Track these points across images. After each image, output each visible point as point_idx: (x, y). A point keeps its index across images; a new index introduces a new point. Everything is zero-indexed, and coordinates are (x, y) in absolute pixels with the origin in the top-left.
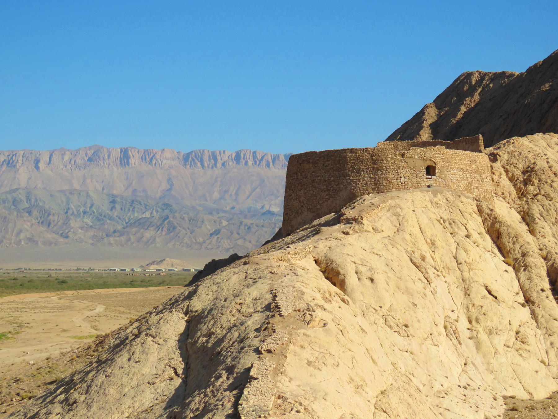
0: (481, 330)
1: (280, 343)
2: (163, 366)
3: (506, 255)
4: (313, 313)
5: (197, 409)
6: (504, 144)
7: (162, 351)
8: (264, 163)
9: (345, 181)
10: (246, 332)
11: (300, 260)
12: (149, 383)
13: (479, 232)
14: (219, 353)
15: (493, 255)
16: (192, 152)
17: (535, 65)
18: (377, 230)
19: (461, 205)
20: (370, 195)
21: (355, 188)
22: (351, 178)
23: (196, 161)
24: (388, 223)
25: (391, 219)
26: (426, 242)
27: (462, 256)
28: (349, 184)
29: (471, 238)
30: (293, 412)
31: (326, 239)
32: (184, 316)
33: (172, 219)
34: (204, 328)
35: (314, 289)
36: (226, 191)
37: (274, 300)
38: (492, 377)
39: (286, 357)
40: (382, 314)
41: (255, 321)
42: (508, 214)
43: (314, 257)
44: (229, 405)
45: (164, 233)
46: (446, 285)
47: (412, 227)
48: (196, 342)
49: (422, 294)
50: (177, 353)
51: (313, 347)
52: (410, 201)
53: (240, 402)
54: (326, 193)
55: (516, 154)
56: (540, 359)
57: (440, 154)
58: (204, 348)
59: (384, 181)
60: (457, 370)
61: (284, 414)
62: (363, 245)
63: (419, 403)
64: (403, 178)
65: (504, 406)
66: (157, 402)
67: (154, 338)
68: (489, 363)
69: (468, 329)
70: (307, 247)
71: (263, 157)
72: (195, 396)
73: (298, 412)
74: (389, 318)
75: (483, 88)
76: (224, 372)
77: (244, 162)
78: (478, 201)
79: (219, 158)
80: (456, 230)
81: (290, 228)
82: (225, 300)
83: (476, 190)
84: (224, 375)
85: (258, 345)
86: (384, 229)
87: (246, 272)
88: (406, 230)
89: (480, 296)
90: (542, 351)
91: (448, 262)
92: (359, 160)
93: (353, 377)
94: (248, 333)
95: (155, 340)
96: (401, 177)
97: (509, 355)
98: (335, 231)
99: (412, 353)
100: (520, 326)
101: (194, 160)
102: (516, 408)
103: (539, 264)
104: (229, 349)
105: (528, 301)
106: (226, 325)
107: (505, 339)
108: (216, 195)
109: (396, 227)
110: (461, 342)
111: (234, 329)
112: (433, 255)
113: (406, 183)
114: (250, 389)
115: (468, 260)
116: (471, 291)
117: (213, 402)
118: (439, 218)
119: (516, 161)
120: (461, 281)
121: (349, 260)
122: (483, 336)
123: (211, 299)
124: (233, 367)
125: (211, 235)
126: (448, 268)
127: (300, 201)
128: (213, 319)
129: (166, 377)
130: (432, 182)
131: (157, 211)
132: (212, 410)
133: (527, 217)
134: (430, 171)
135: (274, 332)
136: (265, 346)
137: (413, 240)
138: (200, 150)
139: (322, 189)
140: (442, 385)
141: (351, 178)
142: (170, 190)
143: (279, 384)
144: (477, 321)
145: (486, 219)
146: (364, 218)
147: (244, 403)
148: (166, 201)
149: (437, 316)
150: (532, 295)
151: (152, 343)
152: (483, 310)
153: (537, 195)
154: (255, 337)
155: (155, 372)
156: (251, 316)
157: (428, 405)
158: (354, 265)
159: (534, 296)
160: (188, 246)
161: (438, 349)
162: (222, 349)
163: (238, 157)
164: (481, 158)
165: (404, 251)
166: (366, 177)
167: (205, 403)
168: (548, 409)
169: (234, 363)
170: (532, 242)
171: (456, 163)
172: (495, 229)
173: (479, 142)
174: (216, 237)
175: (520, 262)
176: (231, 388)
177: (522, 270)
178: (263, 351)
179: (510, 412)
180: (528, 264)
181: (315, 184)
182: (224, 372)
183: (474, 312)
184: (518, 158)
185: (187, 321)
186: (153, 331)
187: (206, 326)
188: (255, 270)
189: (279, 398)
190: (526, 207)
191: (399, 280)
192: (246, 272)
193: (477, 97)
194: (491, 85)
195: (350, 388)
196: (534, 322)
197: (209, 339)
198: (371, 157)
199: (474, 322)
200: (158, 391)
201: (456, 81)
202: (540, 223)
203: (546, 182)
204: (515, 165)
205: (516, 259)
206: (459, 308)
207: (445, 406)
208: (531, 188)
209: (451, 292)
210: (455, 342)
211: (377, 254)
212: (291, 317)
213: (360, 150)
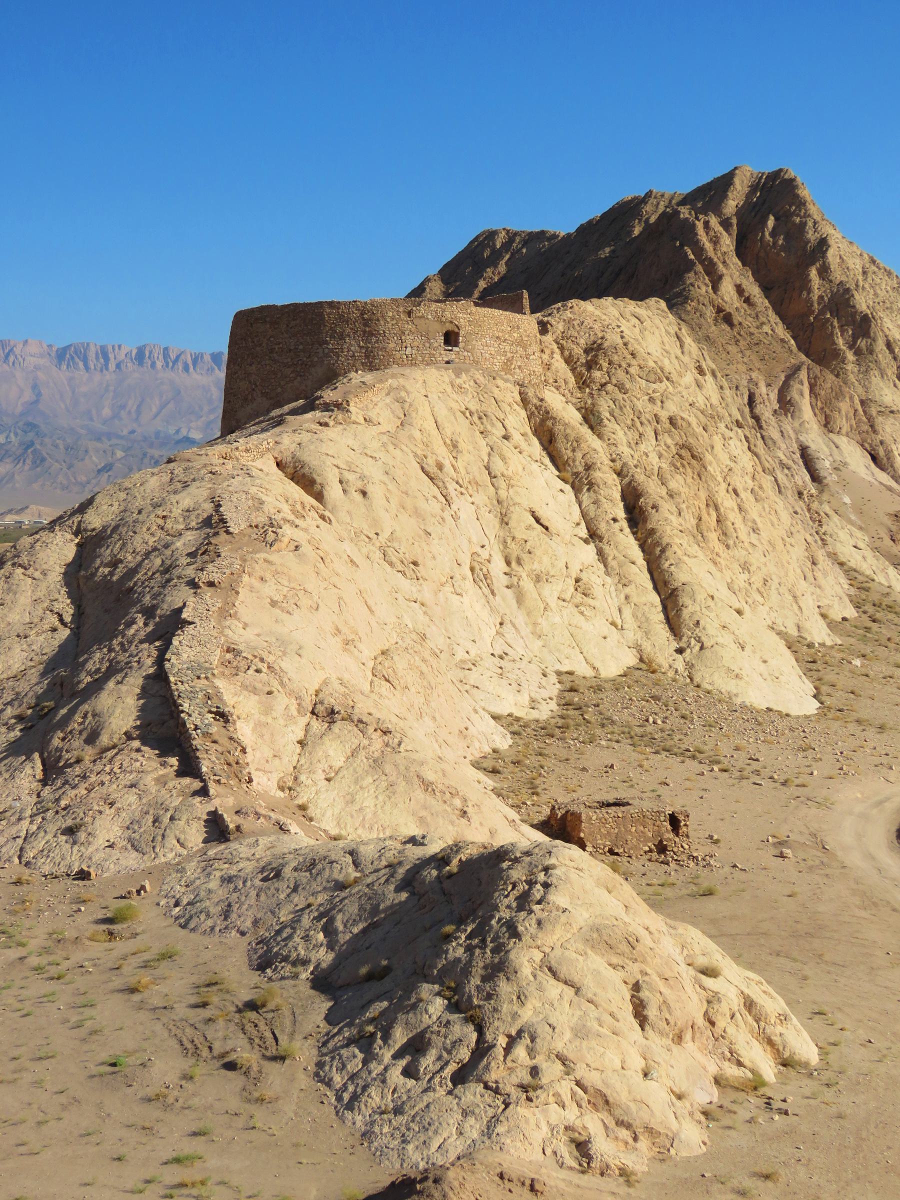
0: (524, 575)
1: (228, 572)
2: (41, 611)
3: (561, 467)
4: (279, 530)
5: (98, 670)
6: (558, 309)
8: (180, 365)
9: (320, 351)
10: (173, 558)
11: (253, 461)
12: (18, 636)
13: (522, 432)
14: (131, 590)
15: (543, 467)
16: (71, 345)
17: (590, 222)
18: (370, 421)
19: (496, 391)
20: (360, 372)
23: (77, 360)
24: (387, 413)
25: (392, 406)
27: (498, 466)
28: (327, 355)
29: (511, 440)
31: (294, 431)
32: (73, 536)
33: (38, 447)
34: (106, 554)
35: (279, 498)
36: (123, 407)
37: (217, 511)
38: (540, 643)
39: (237, 593)
40: (378, 545)
41: (187, 542)
42: (565, 410)
43: (276, 458)
44: (149, 662)
45: (27, 467)
46: (473, 507)
47: (423, 419)
48: (94, 575)
49: (438, 518)
50: (62, 592)
51: (279, 580)
52: (421, 382)
53: (167, 656)
54: (292, 369)
55: (576, 323)
56: (610, 620)
57: (464, 314)
58: (106, 583)
60: (489, 632)
61: (237, 675)
62: (351, 442)
63: (437, 673)
64: (409, 349)
65: (558, 686)
66: (32, 664)
67: (26, 569)
68: (535, 624)
69: (505, 574)
70: (265, 442)
71: (178, 357)
72: (94, 652)
73: (258, 671)
74: (390, 551)
75: (512, 254)
76: (140, 615)
77: (150, 363)
78: (522, 386)
79: (111, 356)
80: (489, 427)
81: (234, 423)
82: (140, 512)
83: (517, 370)
84: (140, 622)
85: (193, 576)
86: (381, 420)
87: (172, 473)
88: (414, 424)
89: (523, 525)
90: (612, 607)
92: (343, 319)
93: (340, 627)
94: (177, 560)
95: (27, 573)
97: (565, 612)
98: (307, 421)
99: (423, 605)
100: (581, 571)
101: (72, 358)
102: (576, 687)
103: (610, 482)
104: (147, 583)
105: (593, 536)
106: (141, 548)
107: (559, 589)
108: (107, 412)
109: (399, 418)
111: (154, 554)
112: (454, 462)
113: (414, 356)
114: (182, 637)
115: (505, 472)
116: (510, 518)
117: (123, 658)
118: (463, 409)
119: (576, 334)
120: (495, 502)
121: (328, 463)
122: (527, 584)
123: (117, 512)
124: (154, 607)
125: (99, 471)
126: (477, 483)
127: (250, 382)
128: (120, 539)
129: (47, 627)
130: (454, 356)
131: (16, 434)
132: (122, 670)
133: (591, 416)
134: (451, 338)
135: (219, 556)
136: (204, 577)
138: (83, 344)
139: (286, 362)
140: (467, 652)
142: (36, 402)
143: (227, 632)
144: (519, 562)
147: (173, 657)
148: (30, 419)
149: (460, 552)
150: (599, 526)
151: (22, 577)
152: (528, 546)
153: (605, 384)
154: (188, 564)
155: (28, 620)
156: (181, 535)
157: (449, 677)
158: (337, 470)
159: (602, 528)
160: (64, 488)
161: (462, 600)
162: (135, 584)
163: (140, 356)
164: (528, 322)
165: (411, 455)
166: (353, 345)
167: (110, 661)
168: (621, 691)
169: (155, 602)
170: (600, 450)
172: (546, 428)
173: (522, 302)
174: (106, 475)
175: (582, 478)
176: (150, 639)
177: (585, 490)
178: (201, 584)
179: (566, 694)
180: (593, 481)
182: (140, 615)
183: (514, 549)
185: (78, 545)
186: (24, 559)
187: (109, 551)
188: (185, 469)
189: (228, 651)
190: (589, 402)
191: (404, 495)
192: (172, 473)
193: (502, 268)
194: (524, 251)
195: (336, 643)
196: (602, 566)
197: (115, 569)
198: (362, 314)
199: (514, 564)
200: (34, 647)
201: (472, 242)
202: (610, 426)
203: (620, 366)
205: (577, 474)
206: (492, 541)
207: (472, 682)
208: (597, 374)
209: (480, 517)
210: (487, 591)
212: (245, 535)
213: (345, 304)
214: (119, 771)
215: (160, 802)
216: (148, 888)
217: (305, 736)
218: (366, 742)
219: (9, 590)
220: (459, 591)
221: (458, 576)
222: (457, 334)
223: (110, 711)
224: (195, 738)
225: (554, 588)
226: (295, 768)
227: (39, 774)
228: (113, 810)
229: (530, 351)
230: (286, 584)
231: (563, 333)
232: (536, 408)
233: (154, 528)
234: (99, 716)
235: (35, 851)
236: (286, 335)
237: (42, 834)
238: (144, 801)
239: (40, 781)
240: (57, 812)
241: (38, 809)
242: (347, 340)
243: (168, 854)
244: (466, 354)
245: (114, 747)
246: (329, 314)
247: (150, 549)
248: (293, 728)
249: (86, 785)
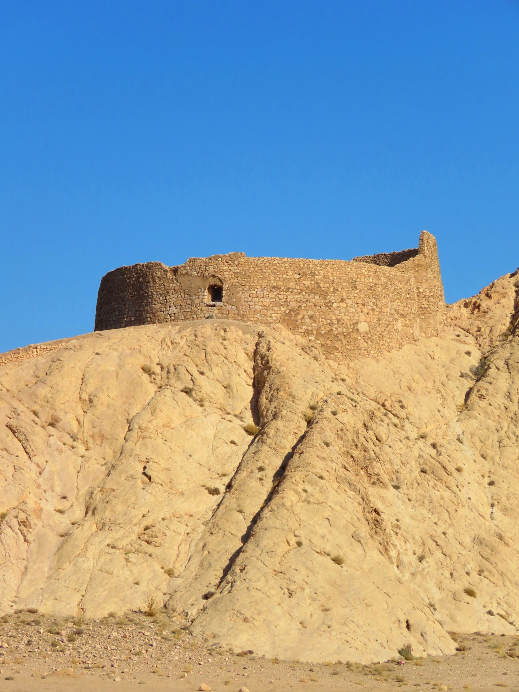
13: (225, 383)
83: (308, 321)
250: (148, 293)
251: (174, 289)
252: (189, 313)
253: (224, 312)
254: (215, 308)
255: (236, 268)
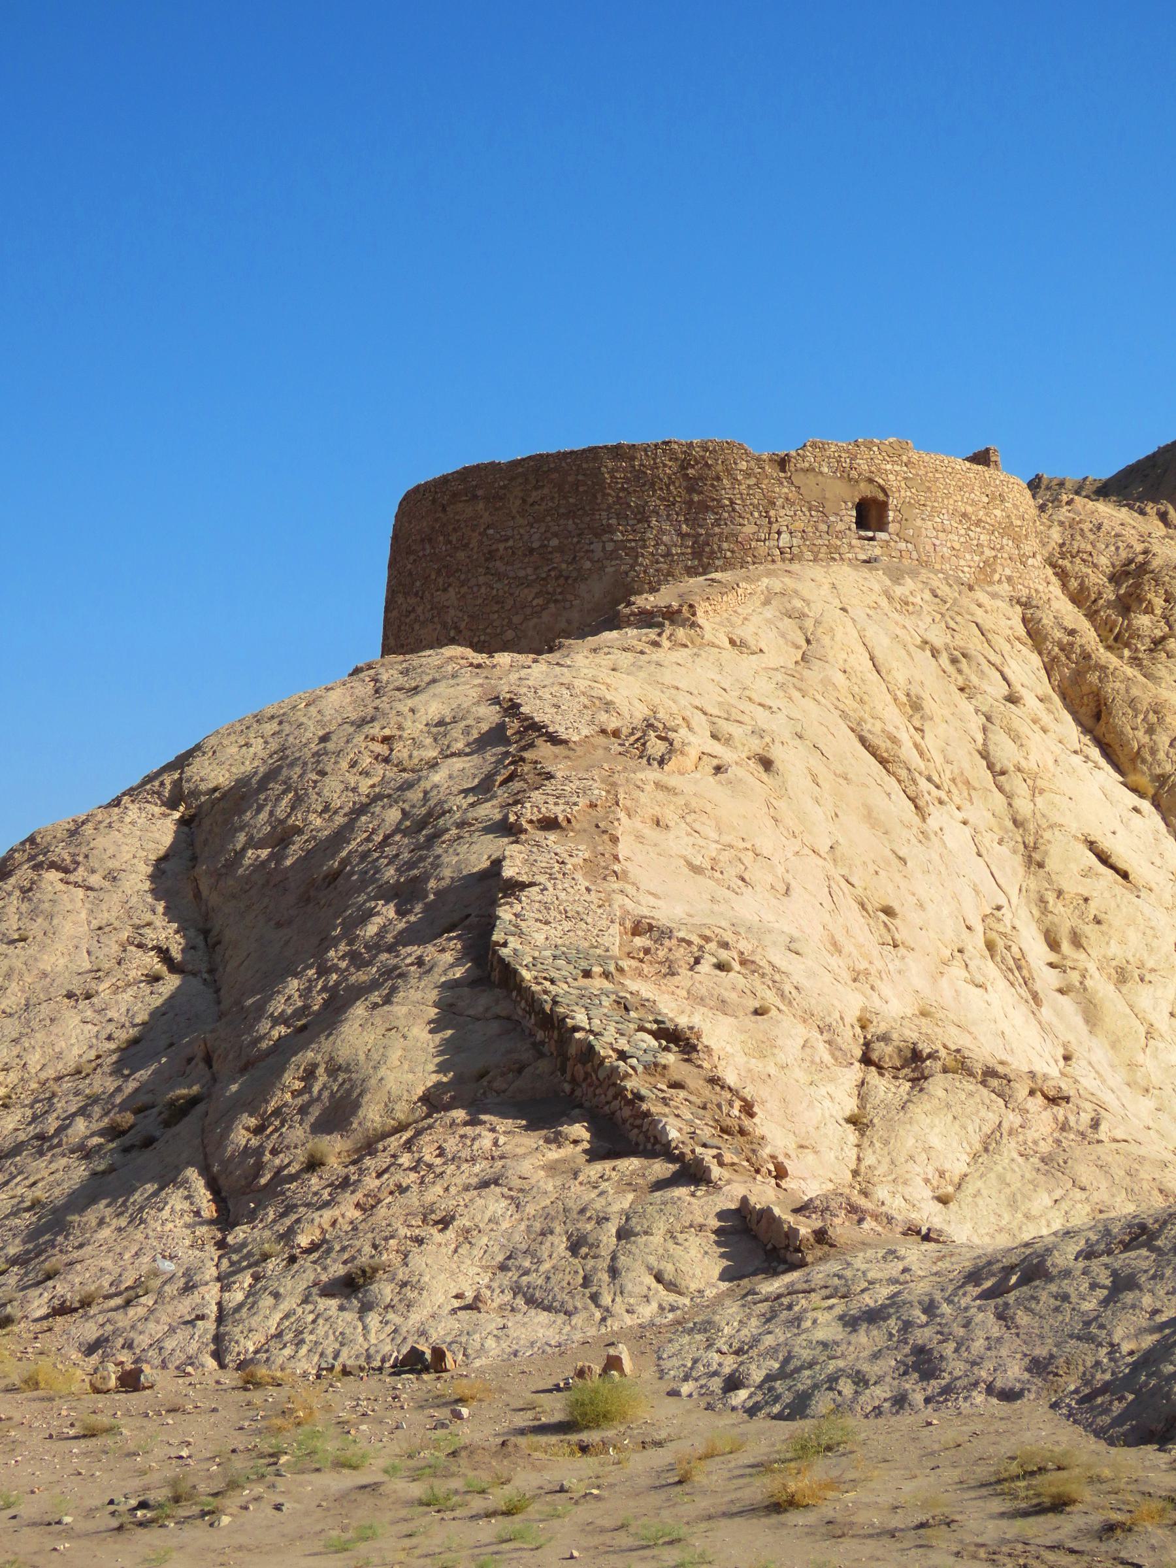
0: (1092, 967)
1: (583, 802)
3: (1126, 765)
4: (671, 735)
7: (104, 906)
9: (596, 547)
12: (70, 995)
14: (335, 876)
19: (979, 612)
21: (632, 567)
22: (619, 536)
25: (780, 625)
26: (895, 700)
27: (1005, 752)
30: (705, 967)
46: (967, 831)
47: (844, 646)
51: (697, 826)
54: (535, 590)
58: (269, 878)
59: (725, 545)
64: (785, 536)
67: (66, 871)
68: (1132, 1066)
69: (1051, 965)
78: (1026, 605)
80: (975, 680)
88: (830, 658)
89: (1075, 868)
91: (966, 765)
92: (641, 480)
96: (779, 533)
106: (341, 800)
109: (798, 647)
110: (1041, 995)
113: (795, 550)
115: (1024, 764)
116: (1046, 853)
119: (1089, 548)
120: (1010, 824)
122: (1101, 986)
126: (967, 783)
127: (444, 625)
128: (284, 792)
130: (878, 551)
137: (856, 688)
141: (619, 536)
144: (1077, 941)
145: (1054, 660)
146: (700, 613)
151: (61, 886)
152: (1093, 909)
155: (87, 966)
166: (665, 533)
171: (948, 496)
172: (1085, 689)
178: (526, 825)
181: (498, 563)
183: (1064, 917)
184: (1092, 537)
189: (636, 931)
191: (841, 781)
198: (683, 467)
199: (1066, 947)
204: (1085, 556)
206: (1014, 900)
208: (1143, 621)
209: (983, 851)
211: (760, 704)
214: (438, 1161)
215: (576, 1208)
216: (627, 1365)
217: (862, 1107)
218: (1012, 1119)
219: (34, 914)
220: (980, 979)
221: (970, 947)
222: (883, 506)
223: (376, 1056)
224: (627, 1075)
225: (1159, 993)
226: (855, 1173)
227: (209, 1210)
228: (450, 1233)
229: (1027, 549)
230: (714, 835)
231: (1062, 545)
232: (1062, 650)
233: (366, 761)
234: (348, 1070)
235: (259, 1338)
236: (520, 521)
237: (267, 1301)
238: (530, 1209)
239: (211, 1222)
240: (292, 1259)
241: (232, 1264)
242: (654, 523)
243: (639, 1304)
244: (902, 545)
245: (400, 1128)
246: (612, 472)
247: (364, 800)
248: (831, 1088)
249: (359, 1196)
250: (719, 501)
251: (787, 499)
252: (824, 549)
253: (893, 554)
254: (875, 543)
255: (905, 469)
